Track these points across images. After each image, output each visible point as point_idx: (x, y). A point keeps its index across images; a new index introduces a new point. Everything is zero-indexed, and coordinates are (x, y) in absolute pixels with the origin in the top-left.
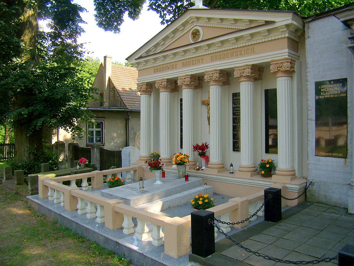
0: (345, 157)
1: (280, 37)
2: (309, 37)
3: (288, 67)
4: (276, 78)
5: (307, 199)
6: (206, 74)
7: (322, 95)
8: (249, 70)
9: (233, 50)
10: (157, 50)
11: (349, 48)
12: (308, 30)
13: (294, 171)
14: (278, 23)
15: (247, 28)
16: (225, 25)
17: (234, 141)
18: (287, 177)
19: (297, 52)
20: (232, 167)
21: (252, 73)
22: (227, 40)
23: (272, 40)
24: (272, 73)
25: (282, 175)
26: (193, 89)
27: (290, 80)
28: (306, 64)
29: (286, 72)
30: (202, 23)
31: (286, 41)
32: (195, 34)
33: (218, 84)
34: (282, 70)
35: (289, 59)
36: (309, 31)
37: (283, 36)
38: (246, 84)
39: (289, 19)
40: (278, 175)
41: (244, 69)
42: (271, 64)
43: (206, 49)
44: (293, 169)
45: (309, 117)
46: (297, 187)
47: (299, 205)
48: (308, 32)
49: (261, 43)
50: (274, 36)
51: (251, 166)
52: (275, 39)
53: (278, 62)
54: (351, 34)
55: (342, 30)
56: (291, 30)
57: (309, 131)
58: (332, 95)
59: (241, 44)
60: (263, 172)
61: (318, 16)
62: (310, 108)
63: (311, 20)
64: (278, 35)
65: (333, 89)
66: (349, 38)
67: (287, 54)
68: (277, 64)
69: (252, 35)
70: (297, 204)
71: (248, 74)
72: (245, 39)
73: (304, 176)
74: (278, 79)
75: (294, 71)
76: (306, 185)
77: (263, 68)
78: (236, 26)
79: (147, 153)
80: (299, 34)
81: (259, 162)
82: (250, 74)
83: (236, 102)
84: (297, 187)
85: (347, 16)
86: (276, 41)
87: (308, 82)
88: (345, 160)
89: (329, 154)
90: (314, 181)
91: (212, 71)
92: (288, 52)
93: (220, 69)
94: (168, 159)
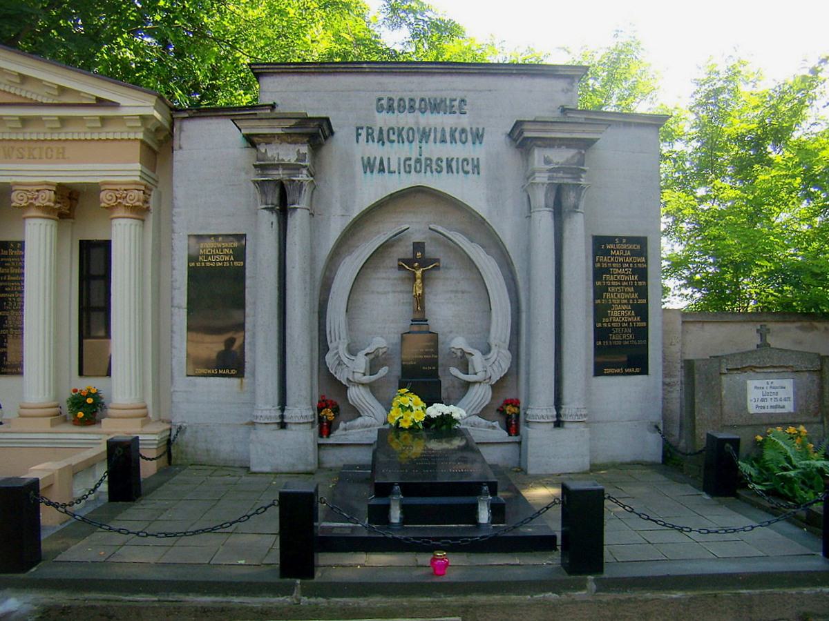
0: (240, 374)
1: (125, 136)
3: (138, 201)
4: (112, 219)
5: (173, 461)
6: (16, 190)
7: (201, 262)
8: (139, 196)
9: (12, 144)
11: (254, 184)
12: (180, 133)
13: (145, 407)
19: (154, 172)
21: (56, 202)
22: (39, 119)
24: (104, 207)
25: (126, 418)
26: (57, 220)
27: (52, 226)
28: (172, 198)
29: (134, 209)
33: (138, 217)
34: (127, 205)
35: (142, 185)
36: (182, 135)
37: (132, 136)
38: (41, 224)
40: (114, 417)
41: (38, 191)
42: (14, 189)
43: (136, 127)
44: (142, 405)
45: (176, 302)
46: (156, 437)
47: (160, 471)
49: (70, 140)
50: (110, 132)
51: (50, 404)
52: (114, 140)
53: (118, 187)
54: (258, 160)
55: (242, 148)
56: (149, 127)
57: (175, 328)
58: (220, 262)
59: (32, 134)
60: (81, 414)
61: (200, 112)
62: (177, 285)
63: (187, 115)
64: (122, 133)
66: (254, 165)
67: (139, 173)
68: (117, 190)
69: (63, 121)
70: (156, 472)
71: (48, 204)
72: (125, 124)
73: (162, 418)
74: (28, 221)
75: (148, 209)
76: (170, 435)
77: (78, 194)
78: (21, 90)
79: (131, 394)
80: (162, 138)
81: (67, 394)
82: (52, 204)
83: (7, 262)
84: (156, 437)
85: (253, 127)
86: (115, 144)
87: (176, 234)
88: (242, 381)
89: (213, 371)
90: (185, 424)
92: (140, 169)
93: (59, 184)
94: (138, 409)
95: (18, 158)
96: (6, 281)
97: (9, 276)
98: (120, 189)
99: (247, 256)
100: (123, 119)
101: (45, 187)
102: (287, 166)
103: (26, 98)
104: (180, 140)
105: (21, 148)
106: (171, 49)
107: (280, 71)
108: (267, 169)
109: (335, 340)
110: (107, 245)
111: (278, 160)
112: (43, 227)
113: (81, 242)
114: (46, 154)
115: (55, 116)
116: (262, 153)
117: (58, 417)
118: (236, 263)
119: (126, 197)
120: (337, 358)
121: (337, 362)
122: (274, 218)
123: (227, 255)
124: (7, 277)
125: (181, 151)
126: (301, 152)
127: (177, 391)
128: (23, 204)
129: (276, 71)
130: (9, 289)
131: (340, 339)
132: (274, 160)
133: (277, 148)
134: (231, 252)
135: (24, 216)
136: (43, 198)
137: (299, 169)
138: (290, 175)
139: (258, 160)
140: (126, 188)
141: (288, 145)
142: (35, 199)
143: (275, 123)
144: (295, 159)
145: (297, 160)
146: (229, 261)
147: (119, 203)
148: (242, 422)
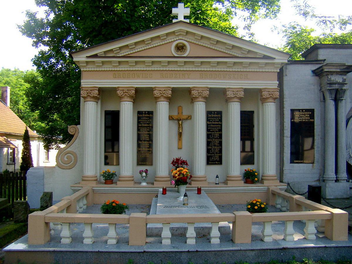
2: (286, 75)
3: (96, 94)
7: (296, 120)
14: (277, 60)
16: (218, 47)
17: (208, 155)
18: (93, 182)
20: (217, 179)
27: (95, 104)
30: (190, 38)
31: (276, 74)
32: (180, 48)
44: (133, 176)
58: (304, 119)
65: (305, 115)
85: (329, 69)
88: (313, 165)
91: (91, 88)
95: (229, 78)
97: (212, 125)
99: (315, 117)
102: (339, 84)
103: (231, 54)
105: (230, 74)
106: (43, 31)
107: (326, 47)
108: (331, 84)
109: (348, 148)
111: (336, 81)
114: (123, 76)
116: (329, 79)
117: (98, 182)
118: (311, 120)
119: (91, 93)
120: (349, 156)
121: (349, 157)
122: (334, 103)
123: (307, 117)
125: (286, 77)
126: (344, 78)
127: (286, 169)
128: (232, 97)
129: (325, 47)
130: (212, 130)
131: (350, 148)
132: (334, 81)
133: (335, 77)
134: (309, 116)
136: (93, 93)
137: (343, 85)
138: (340, 87)
139: (328, 81)
141: (339, 76)
142: (90, 94)
143: (338, 67)
144: (342, 81)
145: (342, 81)
146: (308, 119)
148: (312, 181)
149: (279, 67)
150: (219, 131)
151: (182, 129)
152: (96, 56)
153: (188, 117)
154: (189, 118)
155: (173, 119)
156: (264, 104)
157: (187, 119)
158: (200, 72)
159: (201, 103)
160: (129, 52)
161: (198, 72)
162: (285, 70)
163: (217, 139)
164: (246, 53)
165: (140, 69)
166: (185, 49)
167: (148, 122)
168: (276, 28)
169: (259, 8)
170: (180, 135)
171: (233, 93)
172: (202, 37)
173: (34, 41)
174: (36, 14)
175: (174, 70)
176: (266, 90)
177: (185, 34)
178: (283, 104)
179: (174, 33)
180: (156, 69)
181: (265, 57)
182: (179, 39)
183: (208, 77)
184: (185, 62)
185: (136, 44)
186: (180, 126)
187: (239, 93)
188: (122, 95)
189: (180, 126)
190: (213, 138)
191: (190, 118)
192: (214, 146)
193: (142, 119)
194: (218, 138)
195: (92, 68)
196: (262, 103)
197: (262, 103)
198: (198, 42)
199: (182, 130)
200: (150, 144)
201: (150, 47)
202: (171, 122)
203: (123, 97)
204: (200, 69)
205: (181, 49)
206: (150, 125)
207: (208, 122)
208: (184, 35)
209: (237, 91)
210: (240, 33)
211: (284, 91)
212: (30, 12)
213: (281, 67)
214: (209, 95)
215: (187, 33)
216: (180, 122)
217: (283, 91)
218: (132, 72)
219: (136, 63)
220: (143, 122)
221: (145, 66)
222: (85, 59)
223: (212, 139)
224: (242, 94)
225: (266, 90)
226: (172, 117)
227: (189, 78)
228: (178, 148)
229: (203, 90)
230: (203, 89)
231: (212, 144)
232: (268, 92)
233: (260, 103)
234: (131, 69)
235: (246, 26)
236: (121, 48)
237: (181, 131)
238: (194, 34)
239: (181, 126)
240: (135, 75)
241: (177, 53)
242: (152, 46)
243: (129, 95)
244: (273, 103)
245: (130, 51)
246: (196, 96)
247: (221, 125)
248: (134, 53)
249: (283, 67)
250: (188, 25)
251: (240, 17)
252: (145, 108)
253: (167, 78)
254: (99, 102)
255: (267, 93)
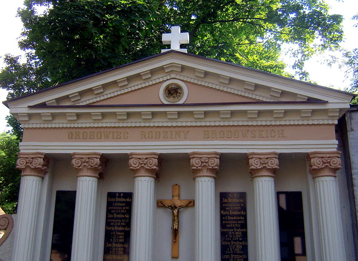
2: (352, 130)
4: (77, 177)
10: (82, 100)
12: (351, 121)
15: (272, 100)
16: (233, 89)
23: (59, 127)
30: (187, 76)
31: (333, 129)
36: (352, 122)
38: (34, 180)
39: (347, 103)
48: (351, 123)
72: (167, 117)
74: (80, 179)
83: (228, 207)
87: (356, 187)
91: (32, 154)
96: (227, 220)
98: (143, 158)
100: (18, 115)
101: (214, 156)
103: (251, 98)
104: (351, 125)
110: (129, 196)
112: (35, 182)
113: (221, 193)
114: (83, 136)
115: (49, 113)
124: (228, 218)
125: (352, 132)
135: (135, 176)
140: (89, 157)
142: (31, 163)
147: (28, 166)
149: (337, 116)
150: (242, 228)
151: (178, 223)
152: (43, 105)
153: (189, 204)
154: (191, 204)
155: (163, 206)
156: (317, 179)
157: (187, 206)
158: (205, 129)
159: (207, 179)
160: (94, 99)
161: (201, 128)
162: (349, 120)
163: (239, 241)
164: (279, 96)
165: (108, 125)
166: (180, 93)
167: (123, 211)
168: (334, 60)
169: (311, 36)
170: (175, 233)
171: (260, 162)
172: (231, 80)
173: (10, 94)
174: (18, 58)
175: (186, 126)
176: (317, 155)
177: (180, 70)
178: (352, 178)
179: (162, 69)
180: (133, 125)
181: (310, 101)
182: (171, 79)
183: (147, 137)
184: (179, 113)
185: (105, 86)
186: (176, 218)
187: (270, 162)
188: (80, 166)
189: (176, 218)
190: (232, 240)
191: (192, 204)
192: (234, 254)
193: (116, 206)
194: (240, 239)
195: (37, 124)
196: (314, 178)
197: (314, 178)
198: (200, 81)
199: (178, 225)
200: (124, 248)
201: (126, 92)
202: (161, 211)
203: (80, 169)
204: (203, 124)
205: (174, 93)
206: (127, 216)
207: (222, 212)
208: (178, 71)
209: (267, 158)
210: (288, 71)
211: (351, 156)
212: (10, 57)
213: (341, 116)
214: (220, 166)
215: (183, 68)
216: (175, 212)
217: (349, 156)
218: (98, 130)
219: (104, 115)
220: (115, 210)
221: (117, 121)
222: (26, 111)
223: (230, 241)
224: (274, 163)
225: (317, 155)
226: (162, 203)
227: (185, 139)
228: (173, 258)
229: (208, 158)
230: (209, 156)
231: (229, 250)
232: (320, 160)
233: (310, 177)
234: (96, 125)
235: (296, 63)
236: (82, 94)
237: (176, 227)
238: (193, 70)
239: (176, 218)
240: (101, 134)
241: (167, 99)
242: (130, 90)
243: (90, 167)
244: (332, 179)
245: (96, 98)
246: (197, 167)
247: (245, 216)
248: (103, 100)
249: (344, 116)
250: (185, 57)
251: (288, 52)
252: (120, 188)
253: (151, 138)
254: (47, 178)
255: (318, 160)
